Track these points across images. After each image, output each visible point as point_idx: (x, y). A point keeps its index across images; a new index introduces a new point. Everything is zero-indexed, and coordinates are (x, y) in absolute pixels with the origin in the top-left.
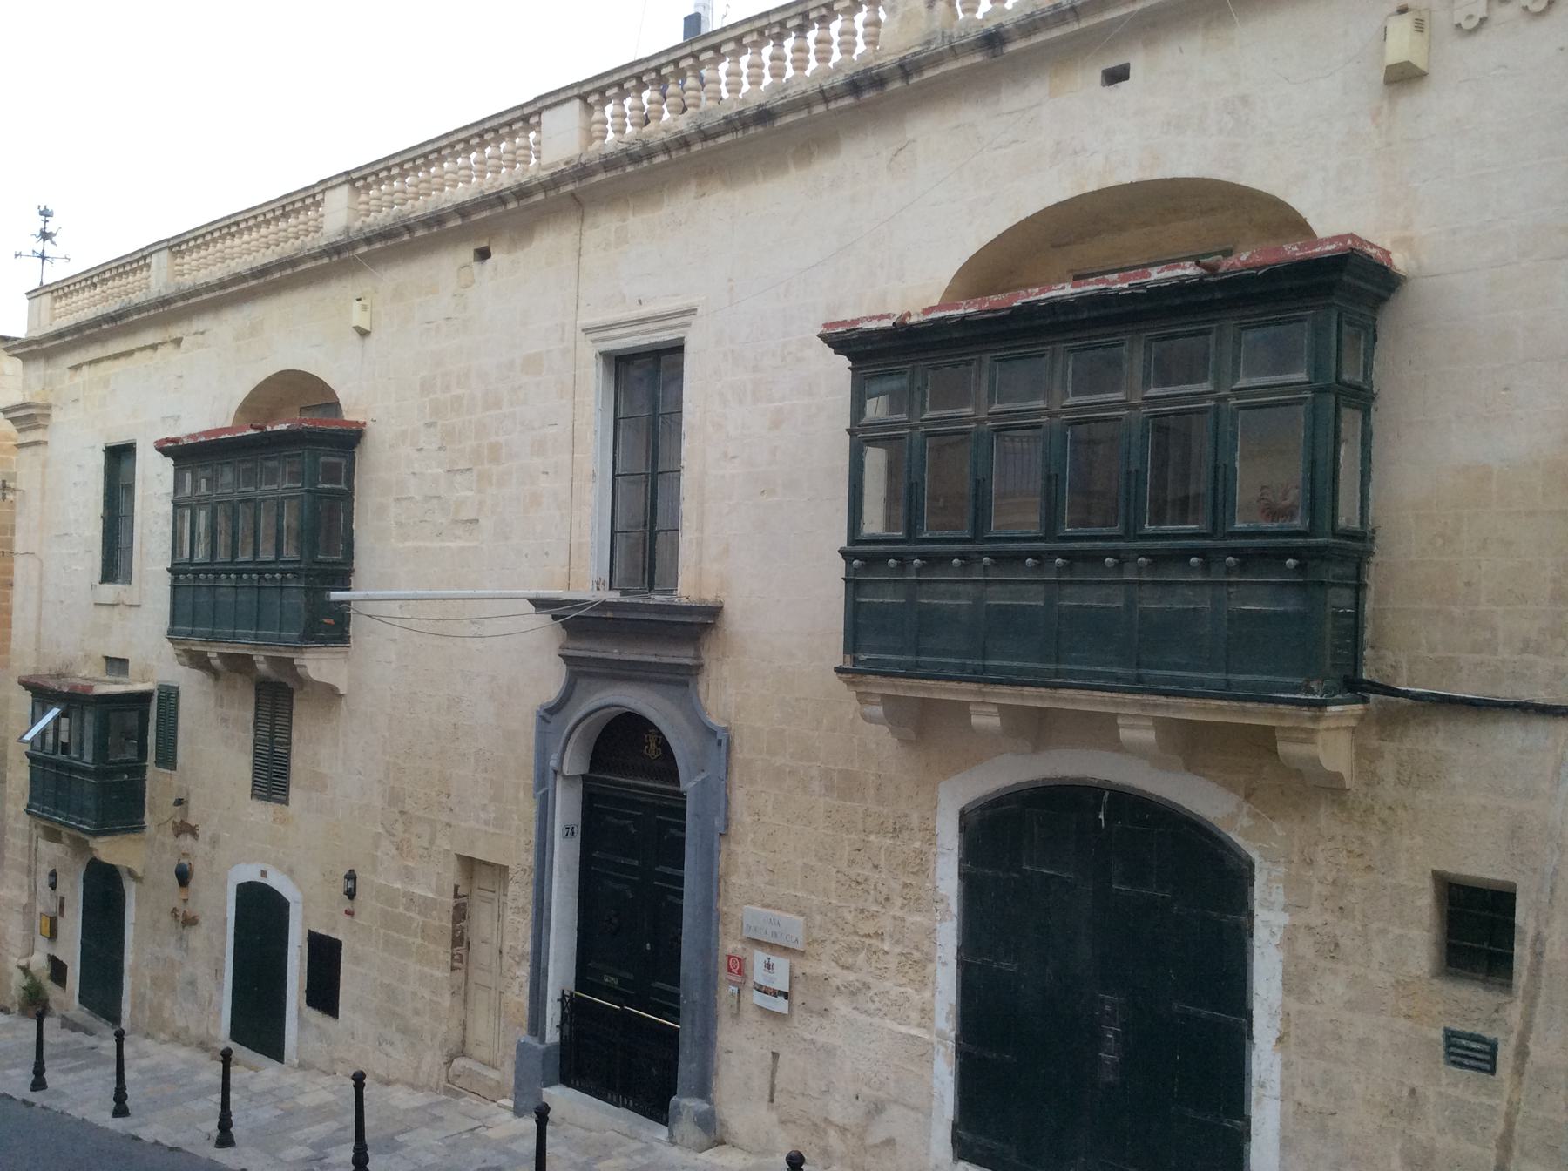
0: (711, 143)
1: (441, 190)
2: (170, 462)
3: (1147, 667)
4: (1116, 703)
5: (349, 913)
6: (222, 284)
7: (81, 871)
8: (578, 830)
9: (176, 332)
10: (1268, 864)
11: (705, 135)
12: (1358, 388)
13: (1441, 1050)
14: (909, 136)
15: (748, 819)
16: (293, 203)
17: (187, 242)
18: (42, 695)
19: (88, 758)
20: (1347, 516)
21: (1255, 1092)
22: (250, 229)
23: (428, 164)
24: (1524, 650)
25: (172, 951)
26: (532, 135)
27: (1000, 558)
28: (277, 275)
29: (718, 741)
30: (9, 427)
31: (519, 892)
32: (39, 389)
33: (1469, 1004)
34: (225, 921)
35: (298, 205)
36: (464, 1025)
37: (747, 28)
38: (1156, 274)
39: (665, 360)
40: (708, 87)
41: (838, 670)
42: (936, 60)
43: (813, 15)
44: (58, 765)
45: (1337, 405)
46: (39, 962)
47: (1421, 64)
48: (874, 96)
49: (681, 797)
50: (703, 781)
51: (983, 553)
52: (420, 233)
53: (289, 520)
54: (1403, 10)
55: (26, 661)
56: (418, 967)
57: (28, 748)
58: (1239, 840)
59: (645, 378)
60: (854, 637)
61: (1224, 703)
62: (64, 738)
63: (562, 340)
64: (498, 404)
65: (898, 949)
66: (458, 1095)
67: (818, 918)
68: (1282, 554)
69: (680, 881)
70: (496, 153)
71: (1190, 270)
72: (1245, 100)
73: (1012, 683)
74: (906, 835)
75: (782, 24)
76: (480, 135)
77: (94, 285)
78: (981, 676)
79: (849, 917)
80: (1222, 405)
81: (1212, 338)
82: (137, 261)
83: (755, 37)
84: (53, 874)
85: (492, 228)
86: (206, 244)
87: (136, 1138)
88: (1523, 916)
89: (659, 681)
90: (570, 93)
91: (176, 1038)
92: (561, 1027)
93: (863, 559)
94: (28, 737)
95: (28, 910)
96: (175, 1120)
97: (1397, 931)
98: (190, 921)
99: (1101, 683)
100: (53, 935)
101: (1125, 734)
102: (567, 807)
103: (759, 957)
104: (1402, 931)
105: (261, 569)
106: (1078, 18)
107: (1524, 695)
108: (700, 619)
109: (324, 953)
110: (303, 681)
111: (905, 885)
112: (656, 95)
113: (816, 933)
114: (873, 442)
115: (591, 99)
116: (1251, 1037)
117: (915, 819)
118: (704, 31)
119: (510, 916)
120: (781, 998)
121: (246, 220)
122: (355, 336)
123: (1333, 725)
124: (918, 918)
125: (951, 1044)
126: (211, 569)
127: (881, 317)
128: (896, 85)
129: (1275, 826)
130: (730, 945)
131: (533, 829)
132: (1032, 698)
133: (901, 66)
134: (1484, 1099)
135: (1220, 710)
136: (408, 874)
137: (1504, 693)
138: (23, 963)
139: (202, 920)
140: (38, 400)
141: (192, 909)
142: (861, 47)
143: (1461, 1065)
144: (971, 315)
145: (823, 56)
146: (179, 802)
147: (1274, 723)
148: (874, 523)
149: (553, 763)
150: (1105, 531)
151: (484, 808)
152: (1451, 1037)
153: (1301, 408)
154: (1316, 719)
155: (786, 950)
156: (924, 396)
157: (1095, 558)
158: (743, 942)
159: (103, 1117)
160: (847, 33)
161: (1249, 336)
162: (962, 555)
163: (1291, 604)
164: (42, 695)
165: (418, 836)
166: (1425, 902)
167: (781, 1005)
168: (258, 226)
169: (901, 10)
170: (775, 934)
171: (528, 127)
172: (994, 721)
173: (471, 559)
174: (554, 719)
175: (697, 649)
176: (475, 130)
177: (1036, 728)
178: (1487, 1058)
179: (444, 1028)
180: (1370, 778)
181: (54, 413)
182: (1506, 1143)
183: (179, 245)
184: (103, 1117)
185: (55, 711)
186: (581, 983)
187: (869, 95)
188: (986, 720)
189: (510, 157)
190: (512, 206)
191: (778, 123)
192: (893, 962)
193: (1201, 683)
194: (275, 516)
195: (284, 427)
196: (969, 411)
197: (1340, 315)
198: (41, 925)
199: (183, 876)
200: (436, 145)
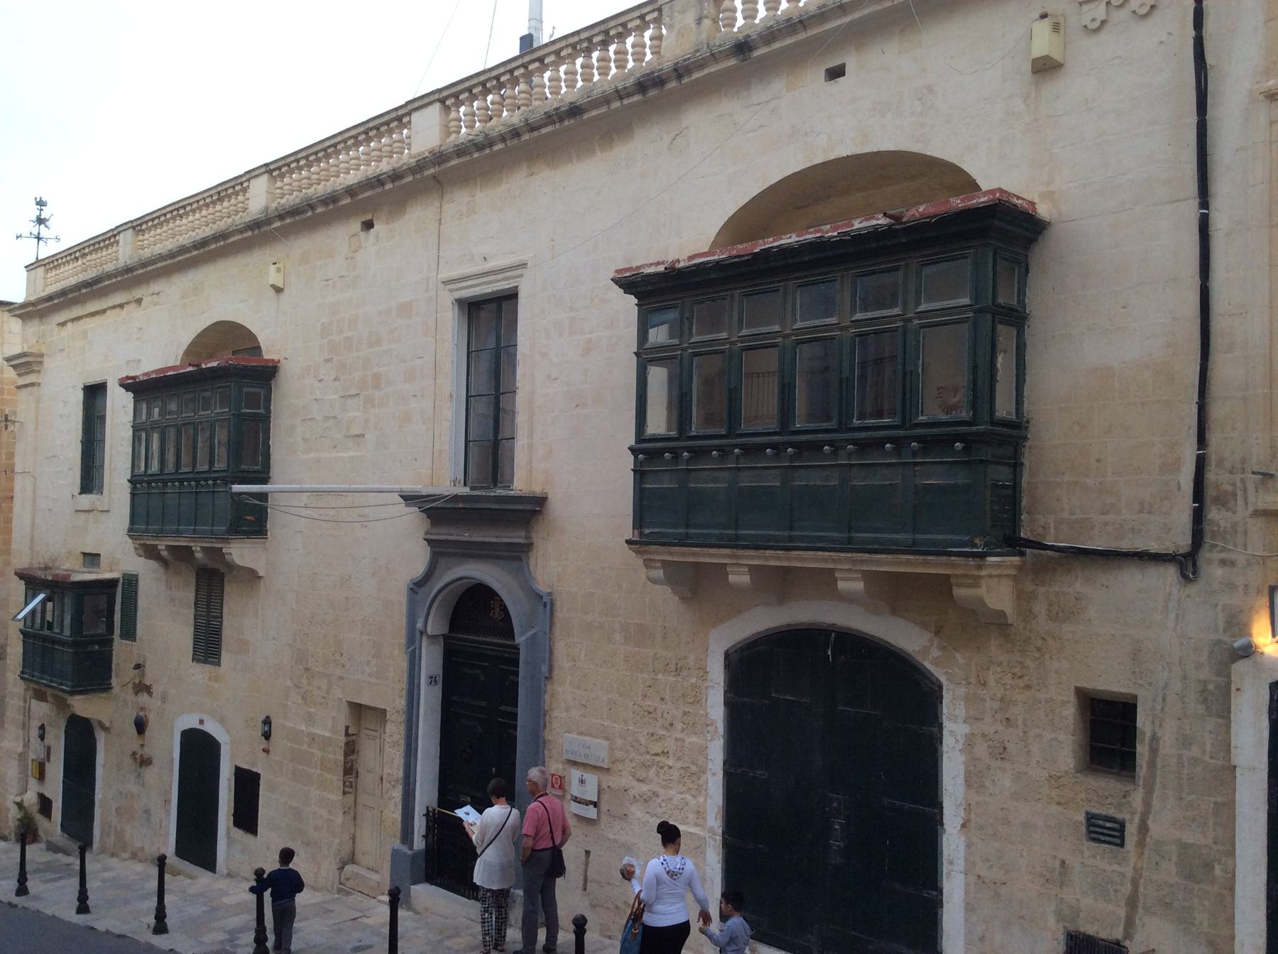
0: (536, 134)
1: (338, 176)
2: (131, 395)
3: (856, 531)
4: (834, 561)
5: (266, 751)
6: (172, 255)
7: (63, 724)
8: (440, 680)
9: (137, 293)
10: (952, 686)
11: (532, 128)
12: (1012, 309)
13: (1084, 829)
14: (684, 125)
15: (567, 665)
16: (226, 190)
17: (146, 222)
18: (32, 582)
19: (67, 632)
20: (1004, 407)
21: (946, 868)
22: (194, 211)
23: (328, 156)
24: (1141, 511)
25: (134, 788)
26: (405, 131)
27: (749, 450)
28: (213, 246)
29: (544, 604)
30: (10, 374)
31: (395, 730)
32: (34, 341)
33: (1103, 793)
34: (172, 760)
35: (230, 191)
36: (354, 839)
37: (563, 44)
38: (857, 225)
39: (505, 305)
40: (536, 90)
41: (628, 542)
42: (701, 65)
43: (612, 33)
44: (44, 639)
45: (993, 322)
46: (30, 798)
47: (1056, 55)
48: (657, 93)
49: (516, 648)
51: (735, 446)
52: (319, 210)
53: (222, 435)
54: (1044, 16)
55: (22, 559)
56: (317, 792)
57: (21, 625)
58: (928, 665)
59: (489, 317)
60: (640, 519)
61: (911, 557)
62: (49, 618)
63: (427, 291)
64: (378, 342)
65: (680, 764)
66: (348, 894)
67: (619, 742)
68: (949, 440)
69: (514, 716)
70: (378, 146)
71: (883, 221)
72: (930, 89)
73: (757, 548)
74: (684, 673)
75: (589, 39)
76: (366, 133)
77: (77, 259)
78: (734, 543)
79: (643, 740)
80: (909, 325)
81: (900, 274)
82: (108, 239)
83: (570, 50)
84: (42, 728)
85: (373, 205)
86: (161, 224)
87: (92, 928)
88: (1143, 721)
89: (498, 557)
90: (432, 98)
91: (134, 856)
92: (426, 837)
93: (648, 453)
94: (20, 616)
95: (22, 757)
96: (120, 914)
97: (1049, 735)
98: (145, 762)
99: (823, 545)
100: (41, 777)
101: (841, 585)
102: (431, 660)
103: (575, 774)
104: (1053, 736)
105: (198, 478)
106: (805, 28)
107: (1140, 545)
108: (529, 507)
109: (247, 783)
110: (231, 566)
111: (685, 713)
112: (497, 98)
113: (618, 754)
114: (651, 361)
115: (448, 103)
116: (942, 824)
117: (691, 660)
118: (535, 45)
119: (388, 749)
120: (591, 807)
121: (191, 204)
122: (272, 293)
123: (995, 572)
124: (694, 739)
125: (719, 838)
126: (162, 479)
127: (658, 264)
128: (672, 85)
129: (958, 655)
131: (405, 676)
132: (773, 559)
133: (675, 70)
134: (1116, 867)
135: (908, 562)
136: (310, 719)
137: (1126, 545)
138: (18, 799)
139: (154, 761)
140: (34, 350)
141: (147, 751)
142: (649, 57)
143: (1099, 841)
144: (723, 260)
145: (621, 64)
146: (138, 667)
147: (948, 572)
148: (658, 423)
149: (419, 625)
150: (825, 425)
151: (368, 663)
152: (1091, 819)
153: (966, 326)
154: (980, 567)
155: (595, 768)
156: (691, 324)
157: (816, 447)
158: (563, 763)
159: (71, 916)
160: (639, 46)
161: (927, 271)
162: (719, 448)
163: (961, 478)
164: (32, 582)
165: (319, 688)
166: (1070, 712)
167: (591, 812)
168: (200, 209)
169: (677, 26)
170: (587, 756)
171: (402, 125)
172: (746, 579)
173: (359, 461)
174: (421, 591)
175: (528, 531)
176: (362, 129)
177: (780, 584)
178: (1117, 834)
179: (338, 841)
180: (1026, 613)
181: (46, 360)
182: (1132, 903)
183: (141, 225)
184: (71, 916)
185: (42, 596)
187: (652, 93)
188: (740, 578)
189: (388, 148)
190: (389, 186)
191: (586, 116)
192: (676, 774)
193: (895, 542)
194: (209, 434)
195: (215, 364)
196: (724, 335)
197: (995, 254)
198: (32, 768)
199: (141, 726)
200: (333, 141)
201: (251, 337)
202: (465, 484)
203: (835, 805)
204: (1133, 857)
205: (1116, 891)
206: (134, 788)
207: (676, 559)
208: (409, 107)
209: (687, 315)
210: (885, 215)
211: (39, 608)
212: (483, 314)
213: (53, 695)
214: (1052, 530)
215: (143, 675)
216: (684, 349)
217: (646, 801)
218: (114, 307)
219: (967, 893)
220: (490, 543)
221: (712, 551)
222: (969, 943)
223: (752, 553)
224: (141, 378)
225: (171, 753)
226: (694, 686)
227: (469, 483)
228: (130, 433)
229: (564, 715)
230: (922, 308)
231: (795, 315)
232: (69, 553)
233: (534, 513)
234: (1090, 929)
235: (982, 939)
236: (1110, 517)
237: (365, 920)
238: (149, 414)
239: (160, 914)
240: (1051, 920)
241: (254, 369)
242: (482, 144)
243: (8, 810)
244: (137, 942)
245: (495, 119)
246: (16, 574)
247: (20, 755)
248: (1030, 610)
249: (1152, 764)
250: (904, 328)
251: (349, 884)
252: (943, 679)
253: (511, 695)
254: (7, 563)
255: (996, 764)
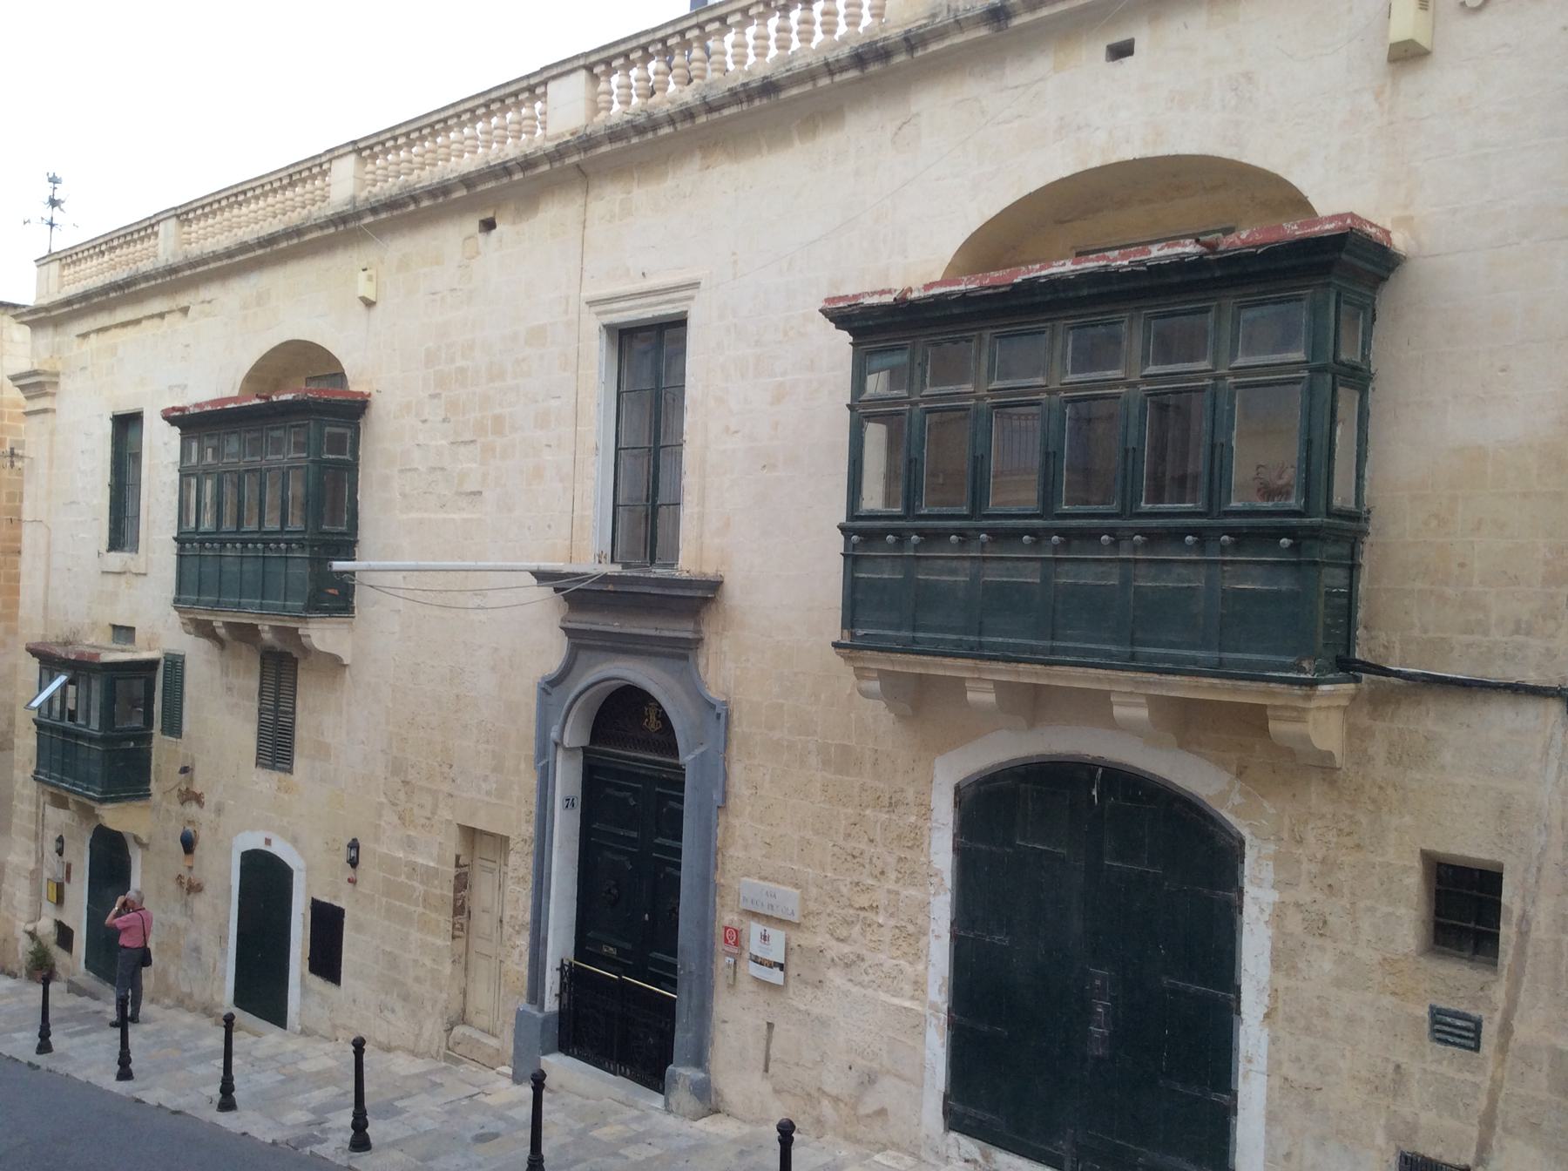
0: (716, 115)
2: (177, 430)
4: (1110, 681)
5: (352, 881)
6: (229, 253)
8: (578, 802)
9: (182, 300)
10: (1256, 842)
11: (710, 107)
12: (1355, 368)
13: (1426, 1027)
15: (746, 792)
16: (300, 172)
17: (195, 210)
18: (49, 662)
20: (1342, 497)
21: (1242, 1067)
22: (257, 198)
23: (434, 134)
24: (1517, 631)
25: (182, 922)
27: (998, 536)
29: (717, 715)
30: (18, 395)
31: (520, 863)
32: (47, 356)
33: (1455, 981)
38: (1156, 252)
39: (668, 334)
41: (836, 645)
42: (940, 33)
44: (66, 732)
45: (1334, 383)
46: (46, 926)
47: (1424, 42)
49: (680, 769)
50: (702, 754)
51: (983, 530)
52: (425, 203)
53: (296, 489)
55: (34, 629)
57: (35, 714)
59: (649, 351)
60: (851, 615)
62: (71, 705)
63: (566, 312)
65: (892, 922)
66: (458, 1062)
67: (814, 891)
69: (678, 852)
70: (502, 123)
71: (1189, 248)
72: (1248, 76)
73: (1008, 660)
74: (901, 809)
76: (486, 105)
77: (102, 253)
78: (977, 652)
79: (844, 890)
80: (1220, 384)
84: (60, 840)
85: (497, 199)
86: (214, 213)
87: (138, 1101)
88: (1510, 896)
89: (656, 654)
90: (576, 64)
92: (560, 996)
93: (861, 534)
94: (35, 704)
95: (35, 875)
97: (1384, 909)
98: (194, 888)
99: (1097, 660)
100: (60, 901)
101: (1118, 711)
102: (567, 779)
103: (755, 929)
104: (1390, 909)
105: (266, 539)
107: (1514, 675)
108: (700, 593)
109: (327, 921)
110: (307, 651)
111: (900, 859)
113: (812, 906)
115: (597, 70)
116: (1239, 1013)
117: (910, 794)
119: (510, 886)
121: (253, 189)
122: (360, 307)
124: (912, 892)
125: (943, 1017)
126: (217, 538)
127: (882, 292)
128: (900, 58)
129: (1266, 804)
130: (727, 917)
131: (534, 799)
132: (1028, 674)
133: (906, 39)
134: (1468, 1076)
135: (1213, 687)
136: (410, 844)
137: (1495, 674)
138: (30, 927)
140: (46, 367)
141: (196, 876)
143: (1446, 1042)
144: (972, 291)
146: (185, 770)
148: (873, 498)
150: (1102, 509)
151: (486, 778)
152: (1437, 1015)
153: (1299, 387)
154: (1308, 698)
157: (1091, 536)
161: (1248, 314)
162: (960, 532)
163: (1285, 584)
164: (49, 662)
165: (421, 806)
166: (1413, 882)
167: (776, 976)
168: (265, 195)
172: (990, 698)
173: (475, 530)
174: (555, 691)
175: (697, 623)
176: (481, 100)
177: (1033, 705)
179: (445, 996)
181: (63, 380)
182: (1488, 1121)
183: (187, 213)
186: (581, 950)
187: (874, 68)
189: (516, 127)
190: (518, 176)
191: (783, 95)
193: (1195, 661)
194: (280, 484)
195: (289, 397)
196: (968, 387)
197: (1339, 294)
199: (188, 844)
200: (442, 115)
201: (338, 363)
202: (613, 561)
203: (1098, 982)
204: (1490, 1067)
205: (1467, 1105)
206: (182, 922)
207: (898, 669)
208: (546, 75)
209: (918, 360)
210: (1197, 241)
211: (58, 694)
212: (639, 346)
213: (77, 803)
214: (1397, 651)
215: (191, 780)
216: (914, 404)
217: (847, 966)
218: (152, 317)
219: (1269, 1099)
220: (647, 637)
221: (948, 661)
222: (1271, 1159)
223: (1001, 666)
224: (192, 410)
225: (229, 878)
226: (914, 827)
227: (617, 559)
228: (176, 476)
229: (741, 854)
230: (1241, 361)
231: (1050, 367)
232: (94, 624)
233: (706, 600)
234: (1432, 1152)
235: (1288, 1156)
236: (1477, 637)
237: (482, 1098)
238: (201, 456)
239: (227, 1087)
240: (1380, 1140)
241: (338, 404)
242: (644, 126)
243: (17, 940)
244: (196, 1121)
245: (658, 94)
246: (28, 650)
247: (32, 872)
248: (1366, 750)
249: (1521, 950)
250: (1214, 387)
251: (459, 1049)
252: (1246, 833)
253: (673, 824)
254: (12, 632)
255: (1310, 941)
